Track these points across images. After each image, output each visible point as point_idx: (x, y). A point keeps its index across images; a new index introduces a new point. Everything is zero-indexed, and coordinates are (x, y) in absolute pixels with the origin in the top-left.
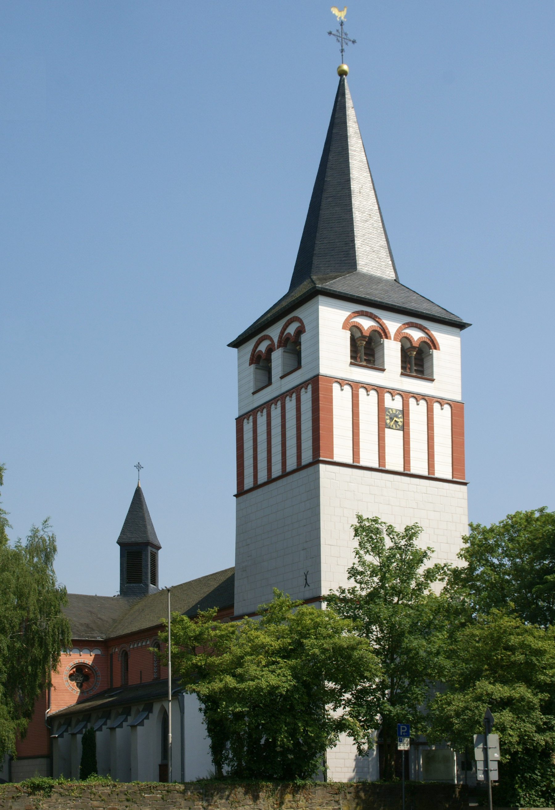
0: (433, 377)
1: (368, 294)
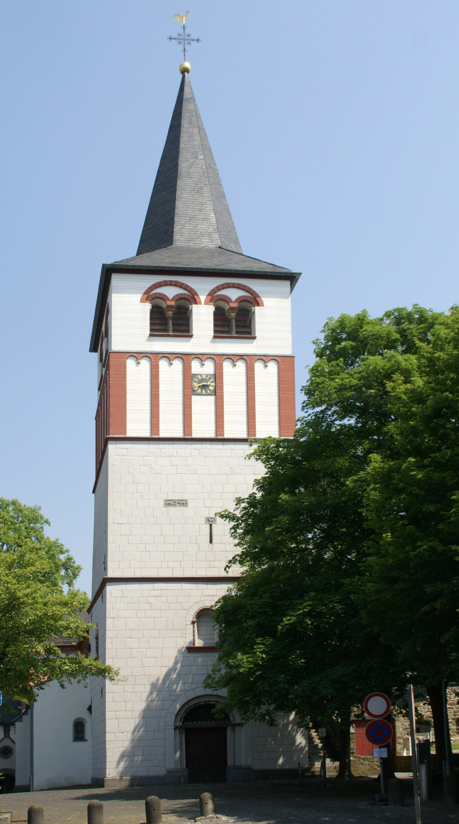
1: (173, 263)
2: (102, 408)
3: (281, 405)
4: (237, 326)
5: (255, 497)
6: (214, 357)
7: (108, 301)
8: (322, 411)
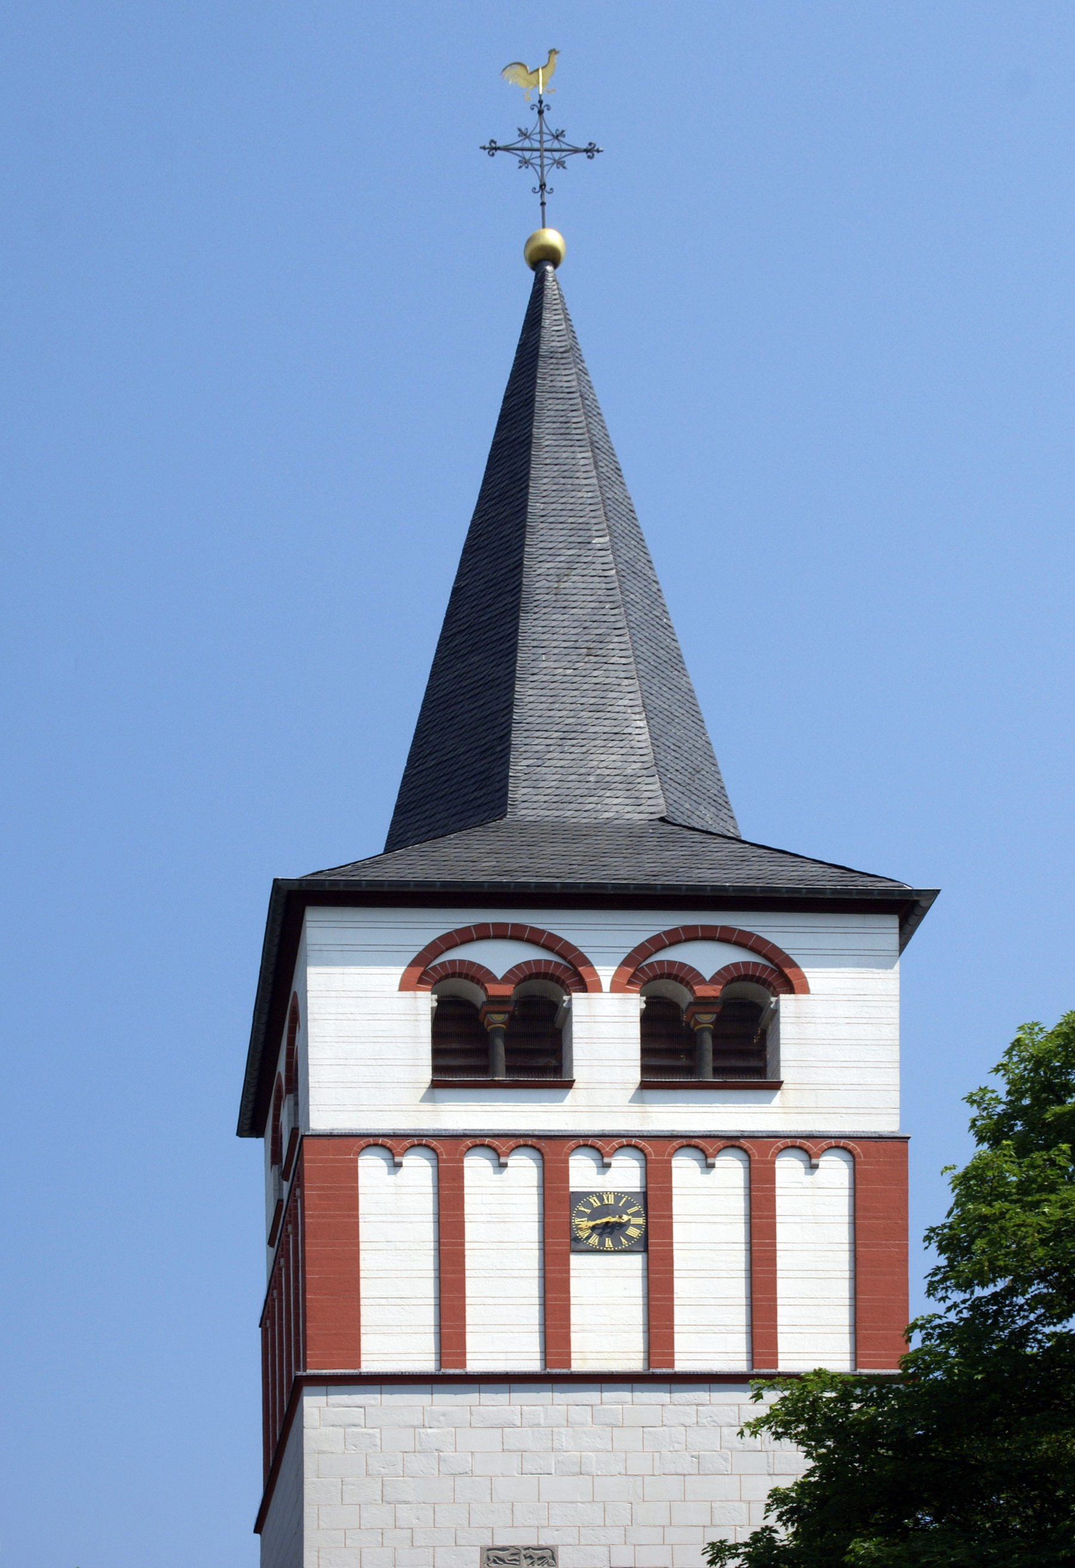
0: (779, 1077)
1: (507, 872)
2: (280, 1294)
3: (861, 1277)
4: (716, 1053)
5: (772, 1540)
6: (642, 1143)
7: (296, 987)
8: (995, 1295)
